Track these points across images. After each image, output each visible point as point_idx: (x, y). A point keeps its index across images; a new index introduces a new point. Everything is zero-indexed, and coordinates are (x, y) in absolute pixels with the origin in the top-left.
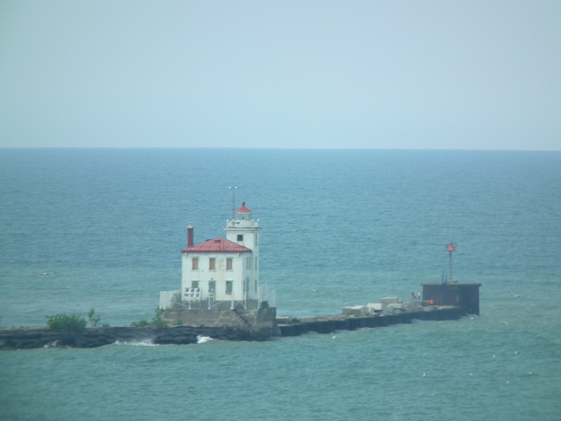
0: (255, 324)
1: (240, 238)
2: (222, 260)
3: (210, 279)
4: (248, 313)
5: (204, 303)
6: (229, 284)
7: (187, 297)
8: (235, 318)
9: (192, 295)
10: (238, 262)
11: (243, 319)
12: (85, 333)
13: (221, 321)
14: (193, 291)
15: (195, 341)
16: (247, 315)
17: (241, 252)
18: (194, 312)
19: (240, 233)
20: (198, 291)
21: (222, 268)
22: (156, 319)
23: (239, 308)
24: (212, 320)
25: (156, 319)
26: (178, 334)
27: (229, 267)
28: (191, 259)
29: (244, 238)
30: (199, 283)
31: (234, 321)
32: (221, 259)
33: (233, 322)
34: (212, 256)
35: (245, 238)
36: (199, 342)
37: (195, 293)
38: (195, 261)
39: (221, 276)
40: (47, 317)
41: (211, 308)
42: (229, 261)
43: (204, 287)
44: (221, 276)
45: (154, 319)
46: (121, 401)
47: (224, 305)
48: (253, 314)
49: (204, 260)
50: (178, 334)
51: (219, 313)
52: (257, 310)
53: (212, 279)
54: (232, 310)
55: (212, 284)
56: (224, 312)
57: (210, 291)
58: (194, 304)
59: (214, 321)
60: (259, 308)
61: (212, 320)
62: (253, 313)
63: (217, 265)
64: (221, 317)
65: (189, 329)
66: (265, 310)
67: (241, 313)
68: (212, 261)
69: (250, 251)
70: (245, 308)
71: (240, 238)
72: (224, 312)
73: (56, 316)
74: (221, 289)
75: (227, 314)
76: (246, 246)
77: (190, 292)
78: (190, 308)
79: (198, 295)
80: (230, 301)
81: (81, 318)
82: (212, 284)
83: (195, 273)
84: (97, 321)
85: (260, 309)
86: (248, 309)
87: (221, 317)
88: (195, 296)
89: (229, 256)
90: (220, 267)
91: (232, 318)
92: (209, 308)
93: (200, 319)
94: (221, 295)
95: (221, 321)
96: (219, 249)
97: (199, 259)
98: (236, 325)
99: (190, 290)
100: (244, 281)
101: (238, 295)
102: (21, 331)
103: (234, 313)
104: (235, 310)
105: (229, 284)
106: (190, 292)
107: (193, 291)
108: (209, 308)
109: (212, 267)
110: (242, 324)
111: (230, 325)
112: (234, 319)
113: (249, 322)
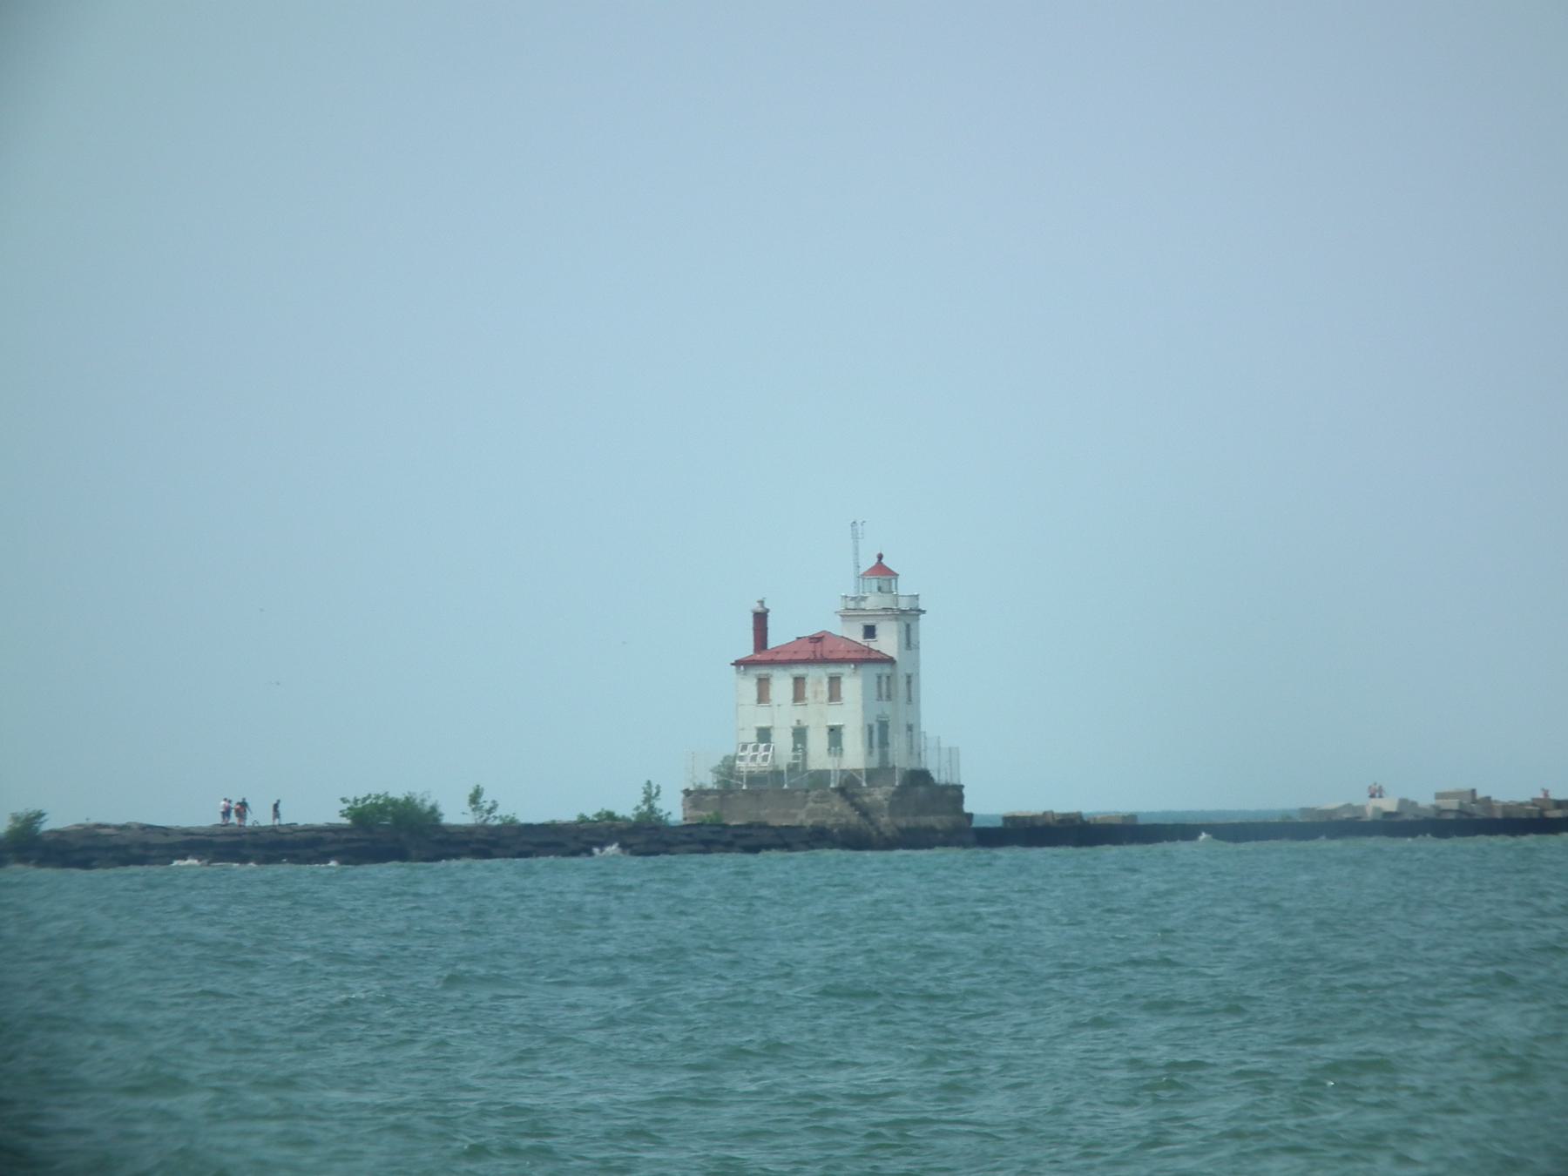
0: (884, 820)
1: (870, 632)
2: (820, 682)
3: (794, 724)
6: (835, 733)
8: (838, 806)
9: (754, 758)
10: (853, 684)
12: (438, 837)
13: (810, 814)
14: (756, 749)
15: (591, 854)
16: (867, 799)
17: (858, 662)
19: (869, 622)
20: (767, 749)
22: (645, 808)
23: (848, 788)
27: (834, 695)
29: (877, 632)
31: (837, 813)
32: (817, 677)
34: (799, 671)
39: (818, 715)
40: (344, 800)
42: (835, 681)
43: (783, 742)
45: (638, 808)
46: (1109, 911)
47: (821, 777)
48: (880, 797)
49: (782, 683)
55: (800, 734)
57: (795, 749)
58: (753, 778)
59: (795, 816)
62: (879, 795)
63: (809, 693)
64: (811, 805)
66: (921, 790)
67: (854, 795)
68: (799, 682)
69: (890, 661)
71: (870, 632)
73: (365, 799)
74: (817, 743)
75: (824, 798)
77: (749, 752)
81: (428, 804)
82: (800, 734)
83: (763, 710)
84: (490, 811)
87: (811, 805)
88: (759, 760)
89: (833, 670)
90: (816, 694)
94: (819, 757)
95: (810, 814)
98: (843, 820)
99: (750, 747)
100: (870, 728)
101: (855, 756)
102: (226, 834)
103: (837, 795)
105: (835, 733)
106: (749, 752)
107: (756, 749)
109: (799, 696)
110: (854, 818)
111: (830, 821)
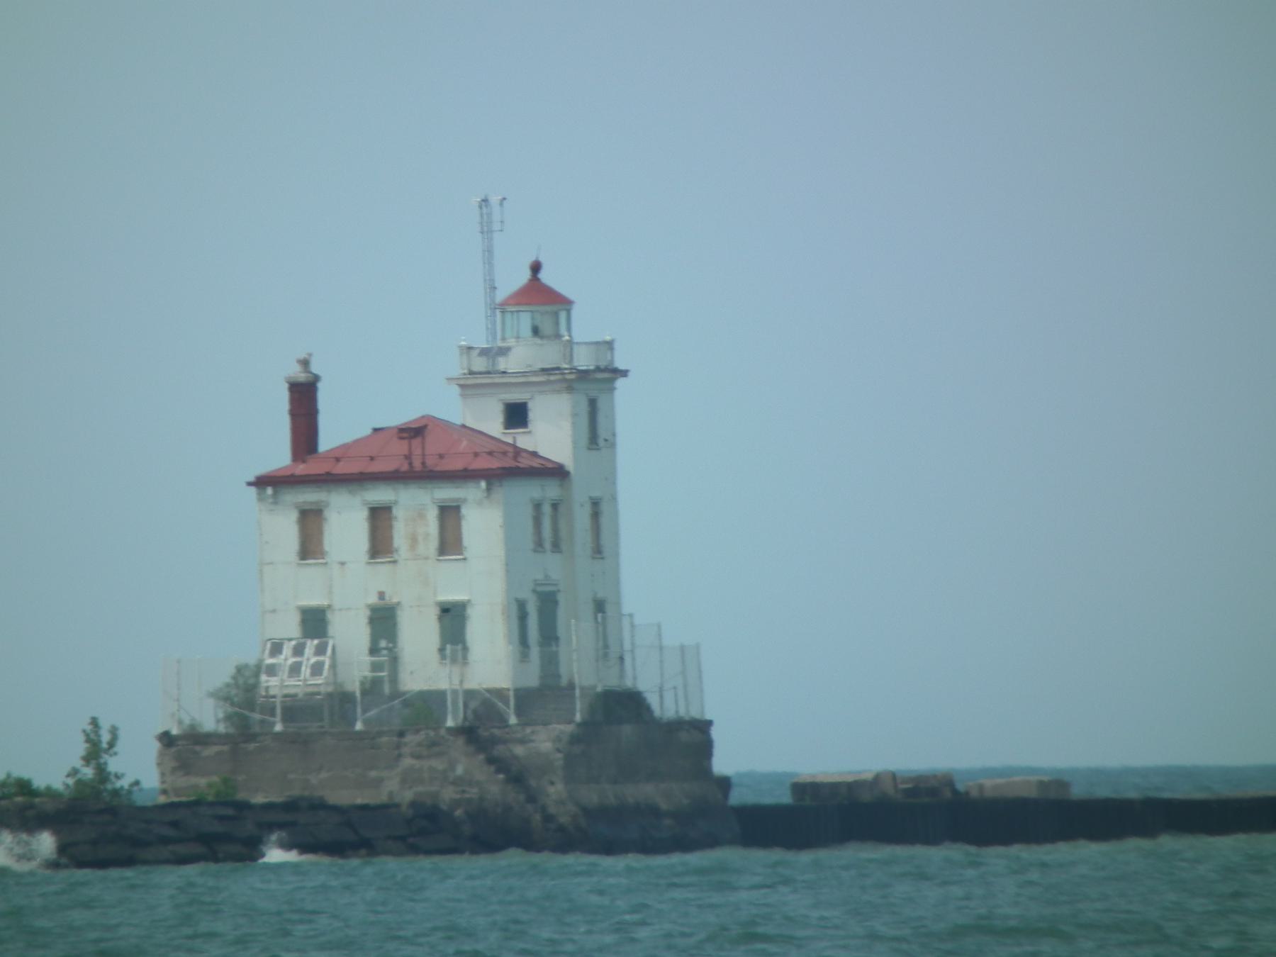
0: (554, 790)
1: (517, 415)
3: (373, 599)
4: (523, 742)
5: (341, 701)
6: (452, 618)
7: (274, 681)
8: (465, 764)
9: (295, 670)
10: (486, 520)
11: (498, 771)
14: (299, 651)
16: (519, 750)
18: (297, 742)
19: (516, 396)
21: (421, 549)
23: (482, 725)
24: (373, 774)
25: (88, 772)
26: (170, 832)
27: (450, 543)
28: (294, 515)
30: (329, 616)
31: (461, 778)
32: (415, 508)
33: (457, 782)
34: (380, 494)
35: (534, 414)
36: (266, 860)
37: (310, 657)
38: (311, 520)
39: (419, 583)
41: (365, 722)
43: (351, 634)
44: (419, 583)
45: (74, 772)
49: (346, 519)
50: (170, 832)
51: (398, 747)
52: (569, 728)
53: (381, 595)
54: (449, 730)
55: (383, 620)
56: (421, 737)
57: (374, 651)
58: (295, 709)
59: (378, 782)
60: (578, 718)
61: (373, 774)
62: (544, 741)
63: (400, 537)
64: (408, 762)
65: (230, 812)
67: (494, 741)
68: (380, 517)
69: (558, 472)
70: (513, 720)
71: (517, 415)
72: (421, 737)
75: (434, 747)
76: (541, 453)
77: (286, 658)
78: (278, 728)
79: (317, 669)
80: (439, 696)
82: (383, 620)
83: (312, 573)
85: (584, 724)
86: (524, 725)
87: (408, 762)
88: (305, 671)
89: (447, 493)
90: (414, 541)
91: (452, 767)
92: (359, 726)
93: (324, 775)
94: (422, 666)
96: (405, 468)
97: (327, 513)
98: (473, 793)
99: (287, 649)
101: (492, 663)
103: (461, 741)
104: (468, 732)
105: (452, 618)
106: (286, 658)
107: (299, 651)
108: (359, 726)
109: (380, 546)
110: (494, 788)
111: (448, 794)
112: (460, 770)
113: (533, 783)
